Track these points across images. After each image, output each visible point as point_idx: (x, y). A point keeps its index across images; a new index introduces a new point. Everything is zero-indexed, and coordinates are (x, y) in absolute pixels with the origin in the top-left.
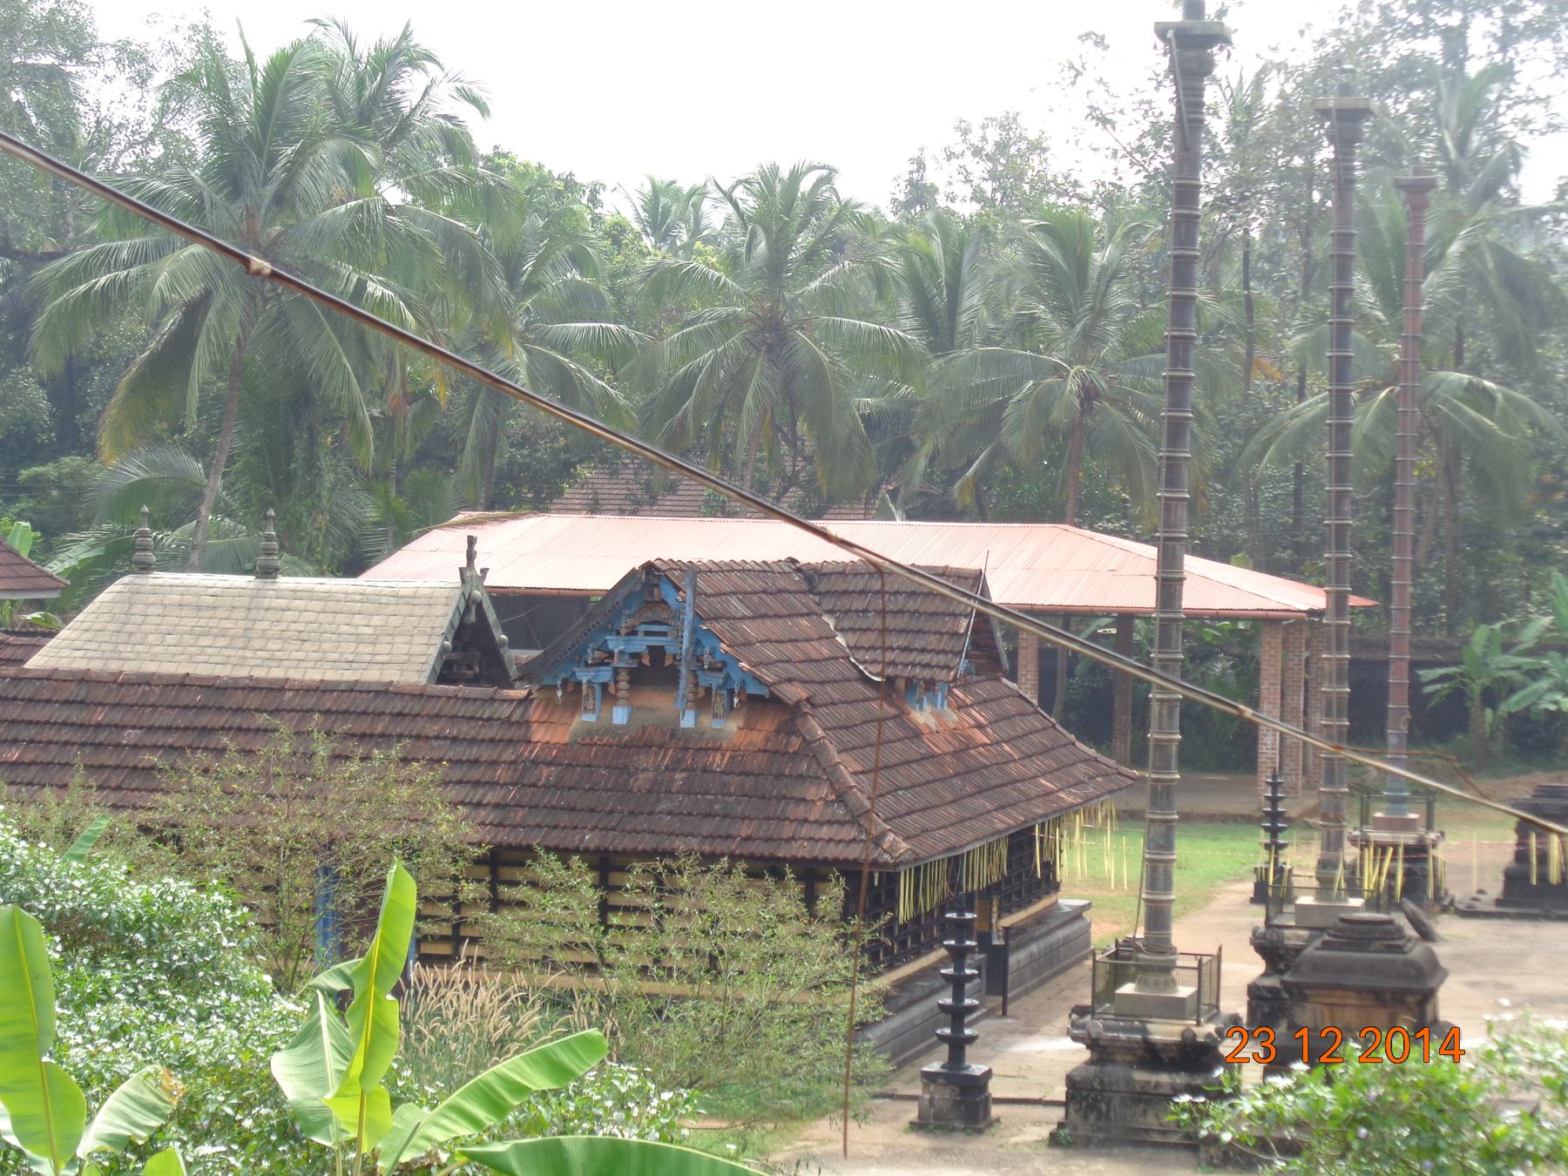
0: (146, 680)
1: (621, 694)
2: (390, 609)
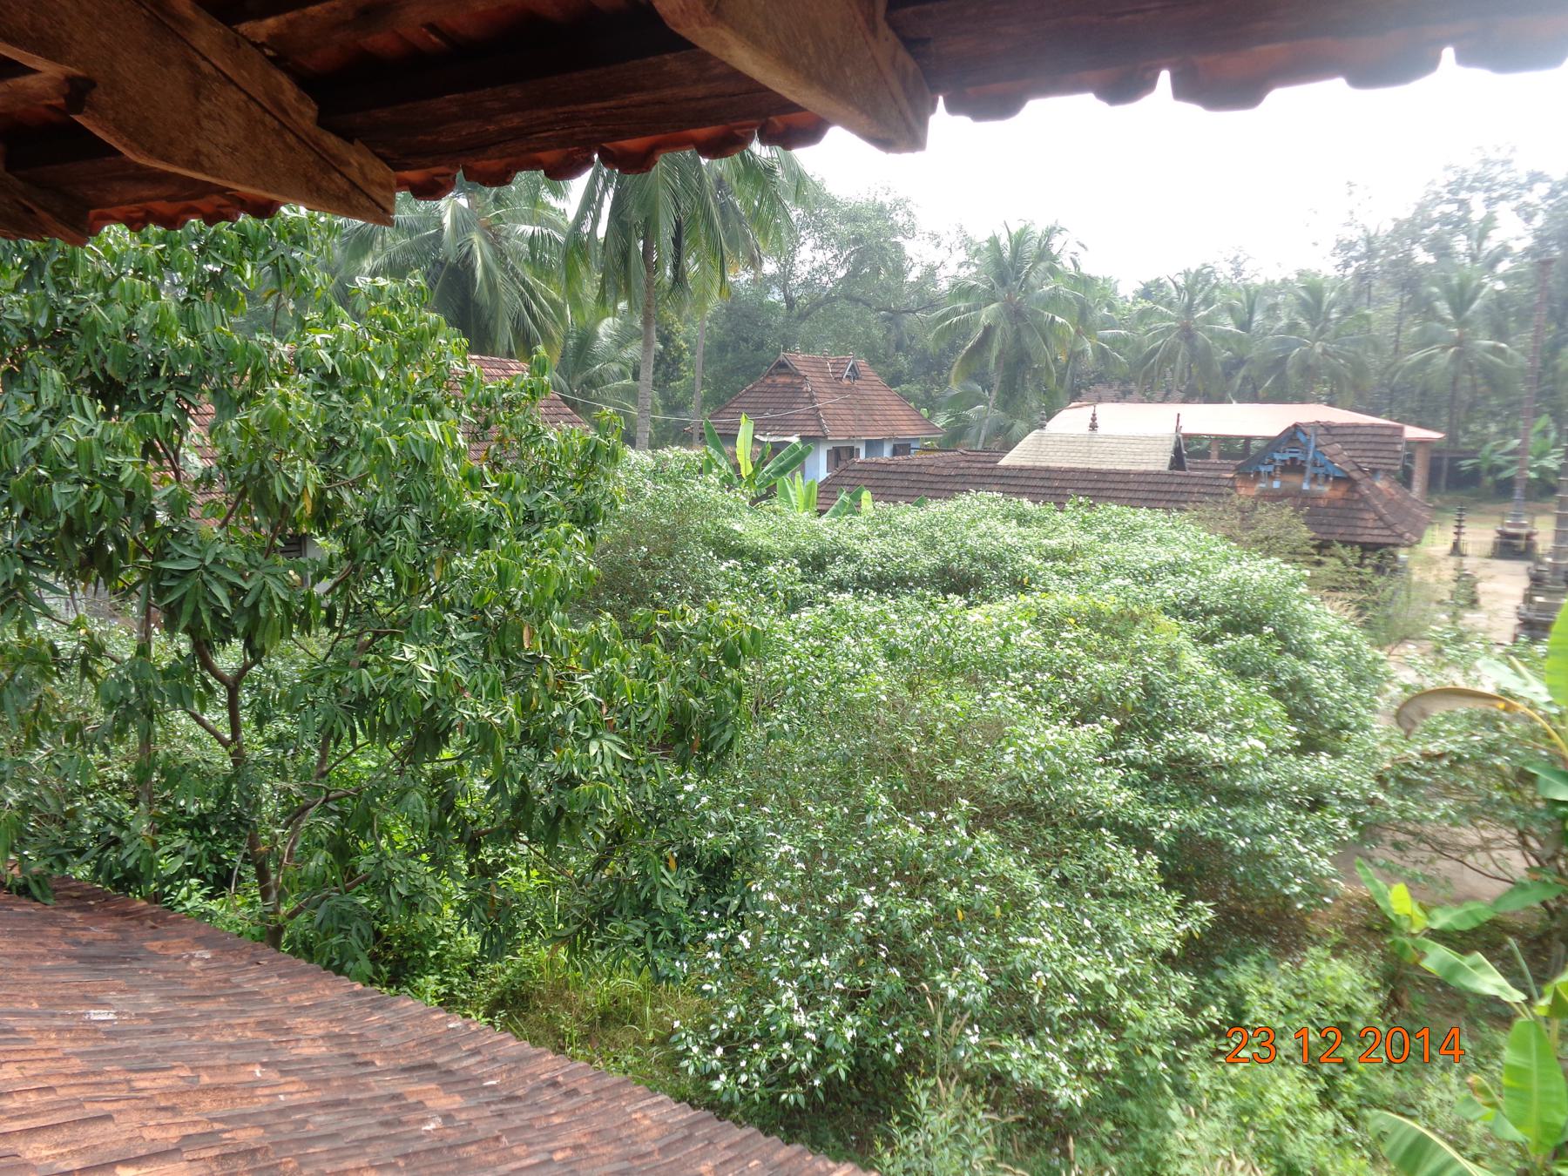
0: (1047, 470)
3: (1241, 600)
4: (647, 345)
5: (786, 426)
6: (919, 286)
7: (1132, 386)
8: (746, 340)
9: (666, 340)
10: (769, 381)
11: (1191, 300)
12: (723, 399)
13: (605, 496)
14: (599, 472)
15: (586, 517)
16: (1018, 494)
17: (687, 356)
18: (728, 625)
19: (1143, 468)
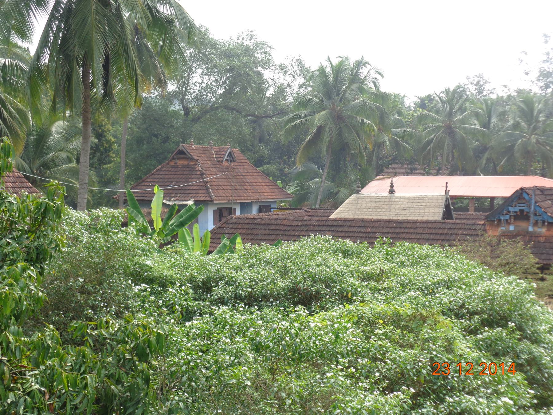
0: (363, 220)
1: (512, 222)
2: (427, 201)
3: (492, 304)
4: (86, 138)
5: (185, 193)
6: (274, 99)
7: (417, 165)
8: (156, 136)
9: (100, 136)
10: (172, 163)
11: (451, 109)
12: (140, 176)
13: (51, 242)
14: (47, 225)
15: (37, 257)
16: (343, 237)
17: (115, 146)
18: (140, 332)
19: (425, 218)
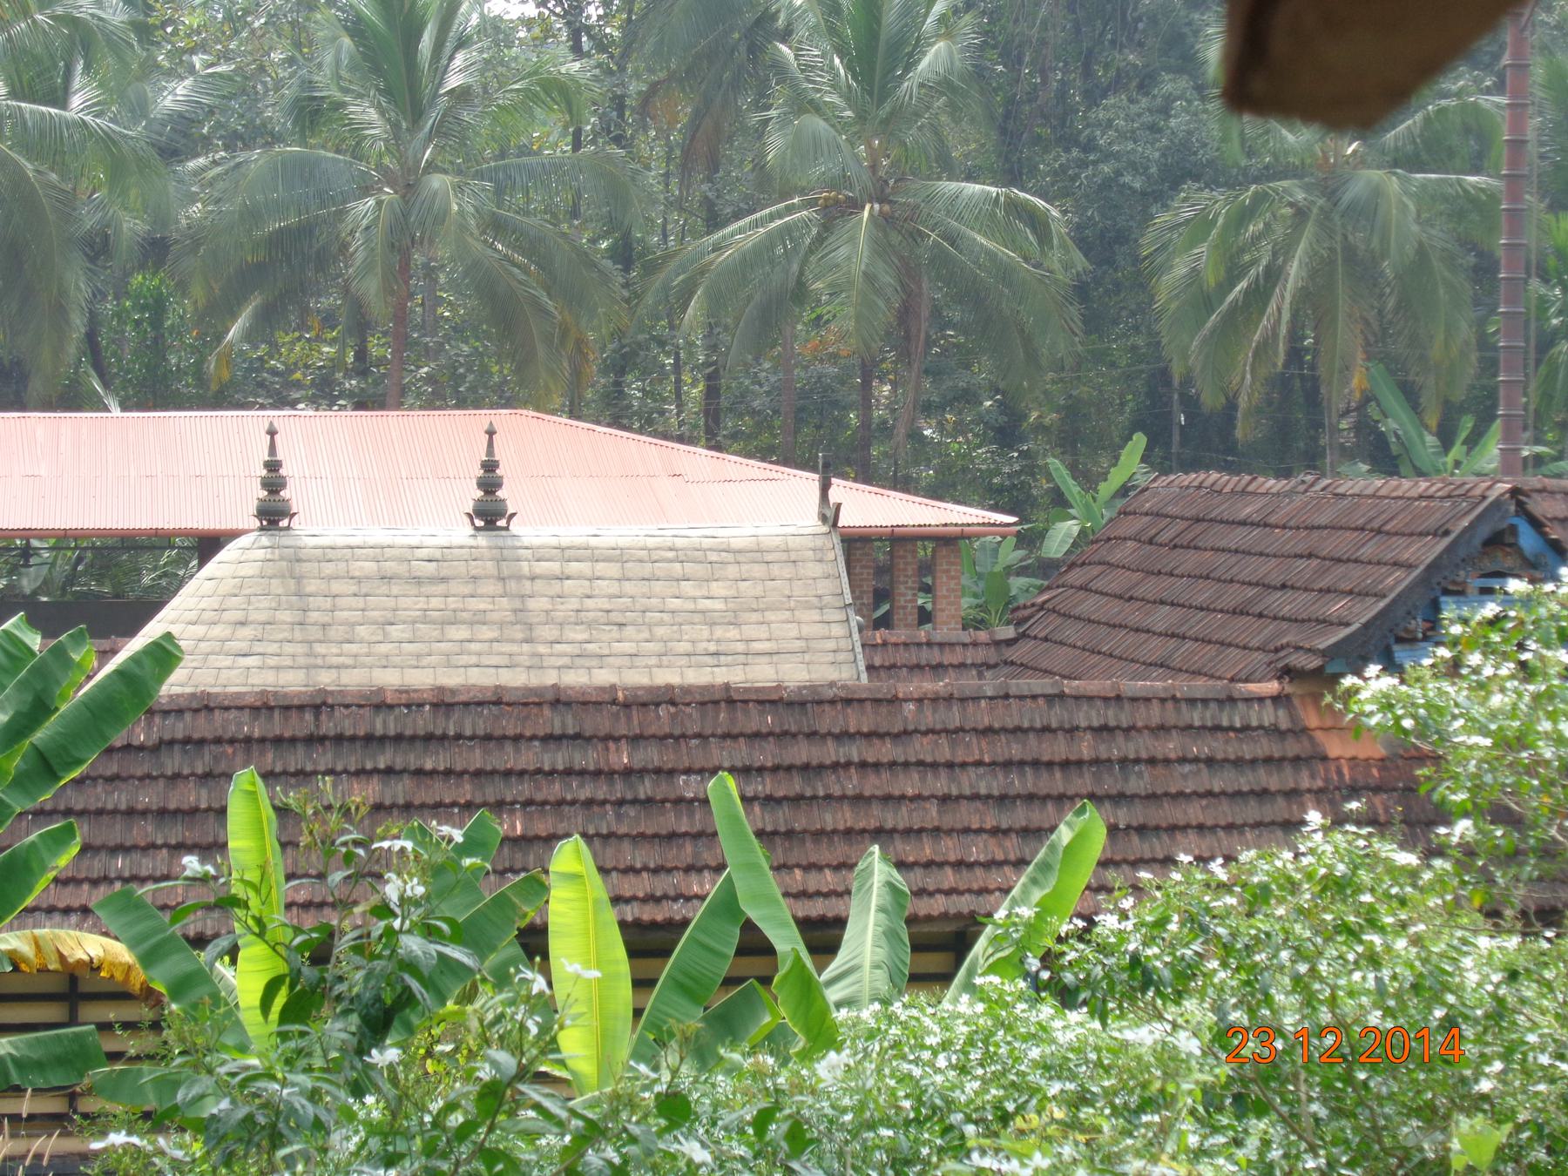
2: (732, 571)
